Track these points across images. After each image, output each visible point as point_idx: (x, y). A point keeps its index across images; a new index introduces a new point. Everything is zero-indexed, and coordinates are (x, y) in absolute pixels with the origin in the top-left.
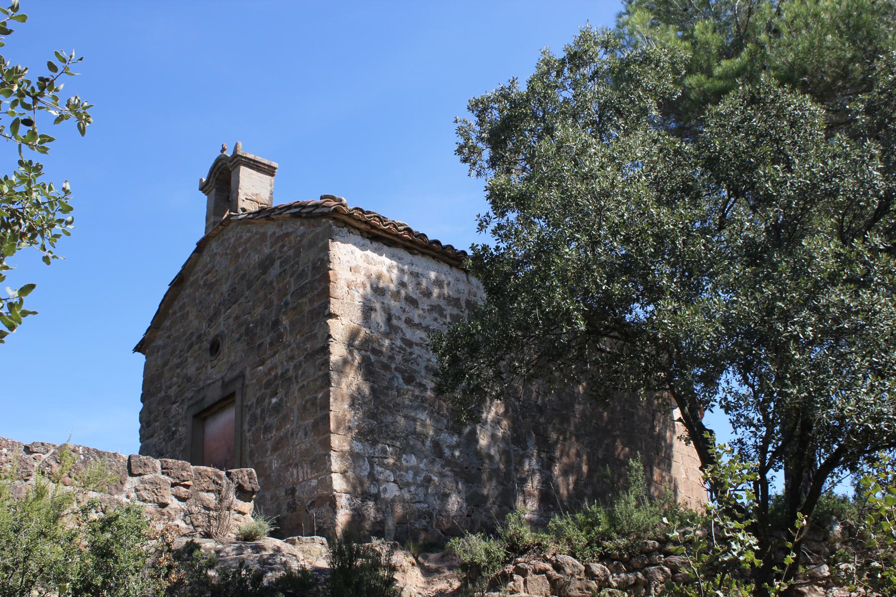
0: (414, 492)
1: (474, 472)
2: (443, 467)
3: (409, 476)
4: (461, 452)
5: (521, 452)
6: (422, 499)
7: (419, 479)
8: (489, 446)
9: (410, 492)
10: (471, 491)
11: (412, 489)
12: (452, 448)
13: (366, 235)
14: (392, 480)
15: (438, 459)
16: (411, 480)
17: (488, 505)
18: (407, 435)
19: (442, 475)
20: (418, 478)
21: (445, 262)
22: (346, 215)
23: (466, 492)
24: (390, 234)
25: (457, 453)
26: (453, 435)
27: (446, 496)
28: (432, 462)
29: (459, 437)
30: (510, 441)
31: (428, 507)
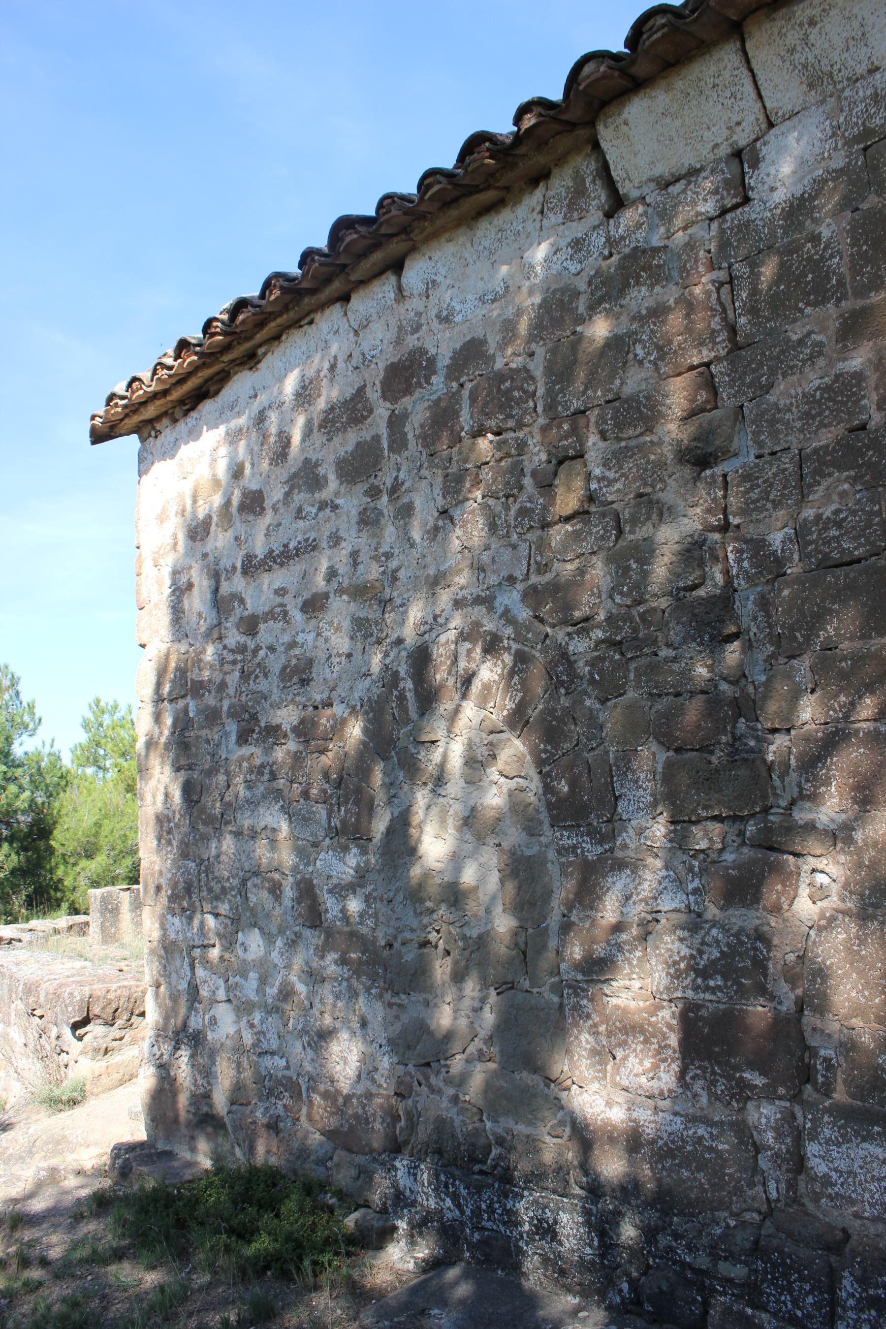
0: (258, 1028)
1: (410, 955)
2: (321, 952)
3: (250, 986)
4: (367, 899)
5: (592, 851)
6: (274, 1047)
7: (272, 991)
8: (456, 860)
9: (252, 1026)
10: (405, 1019)
11: (257, 1017)
12: (341, 891)
13: (178, 412)
14: (224, 998)
15: (307, 933)
16: (253, 997)
17: (457, 1064)
18: (244, 882)
19: (314, 977)
20: (268, 990)
21: (322, 307)
22: (127, 416)
23: (386, 1024)
24: (182, 380)
25: (354, 905)
26: (345, 849)
27: (325, 1036)
28: (292, 944)
29: (364, 851)
30: (544, 817)
31: (287, 1068)
